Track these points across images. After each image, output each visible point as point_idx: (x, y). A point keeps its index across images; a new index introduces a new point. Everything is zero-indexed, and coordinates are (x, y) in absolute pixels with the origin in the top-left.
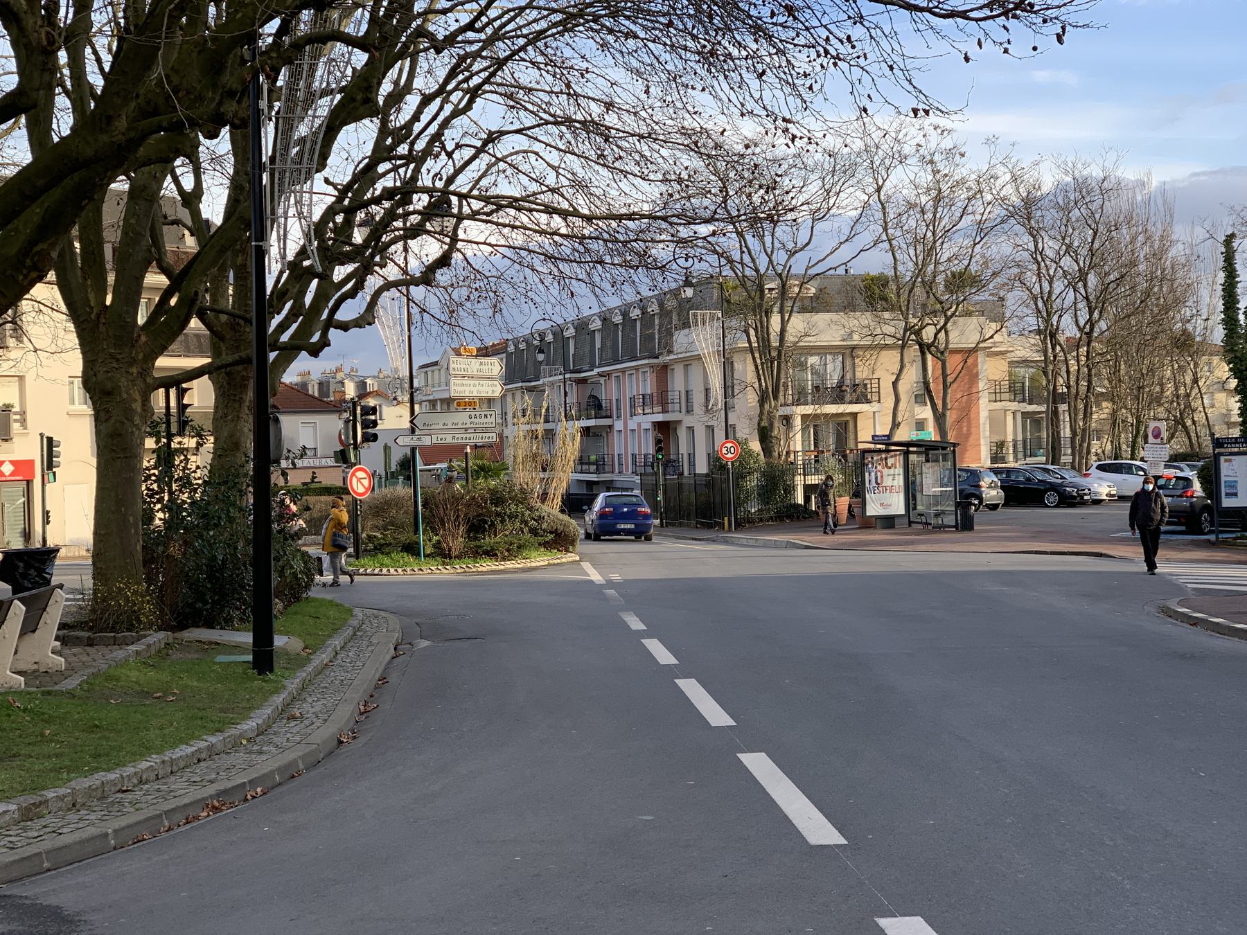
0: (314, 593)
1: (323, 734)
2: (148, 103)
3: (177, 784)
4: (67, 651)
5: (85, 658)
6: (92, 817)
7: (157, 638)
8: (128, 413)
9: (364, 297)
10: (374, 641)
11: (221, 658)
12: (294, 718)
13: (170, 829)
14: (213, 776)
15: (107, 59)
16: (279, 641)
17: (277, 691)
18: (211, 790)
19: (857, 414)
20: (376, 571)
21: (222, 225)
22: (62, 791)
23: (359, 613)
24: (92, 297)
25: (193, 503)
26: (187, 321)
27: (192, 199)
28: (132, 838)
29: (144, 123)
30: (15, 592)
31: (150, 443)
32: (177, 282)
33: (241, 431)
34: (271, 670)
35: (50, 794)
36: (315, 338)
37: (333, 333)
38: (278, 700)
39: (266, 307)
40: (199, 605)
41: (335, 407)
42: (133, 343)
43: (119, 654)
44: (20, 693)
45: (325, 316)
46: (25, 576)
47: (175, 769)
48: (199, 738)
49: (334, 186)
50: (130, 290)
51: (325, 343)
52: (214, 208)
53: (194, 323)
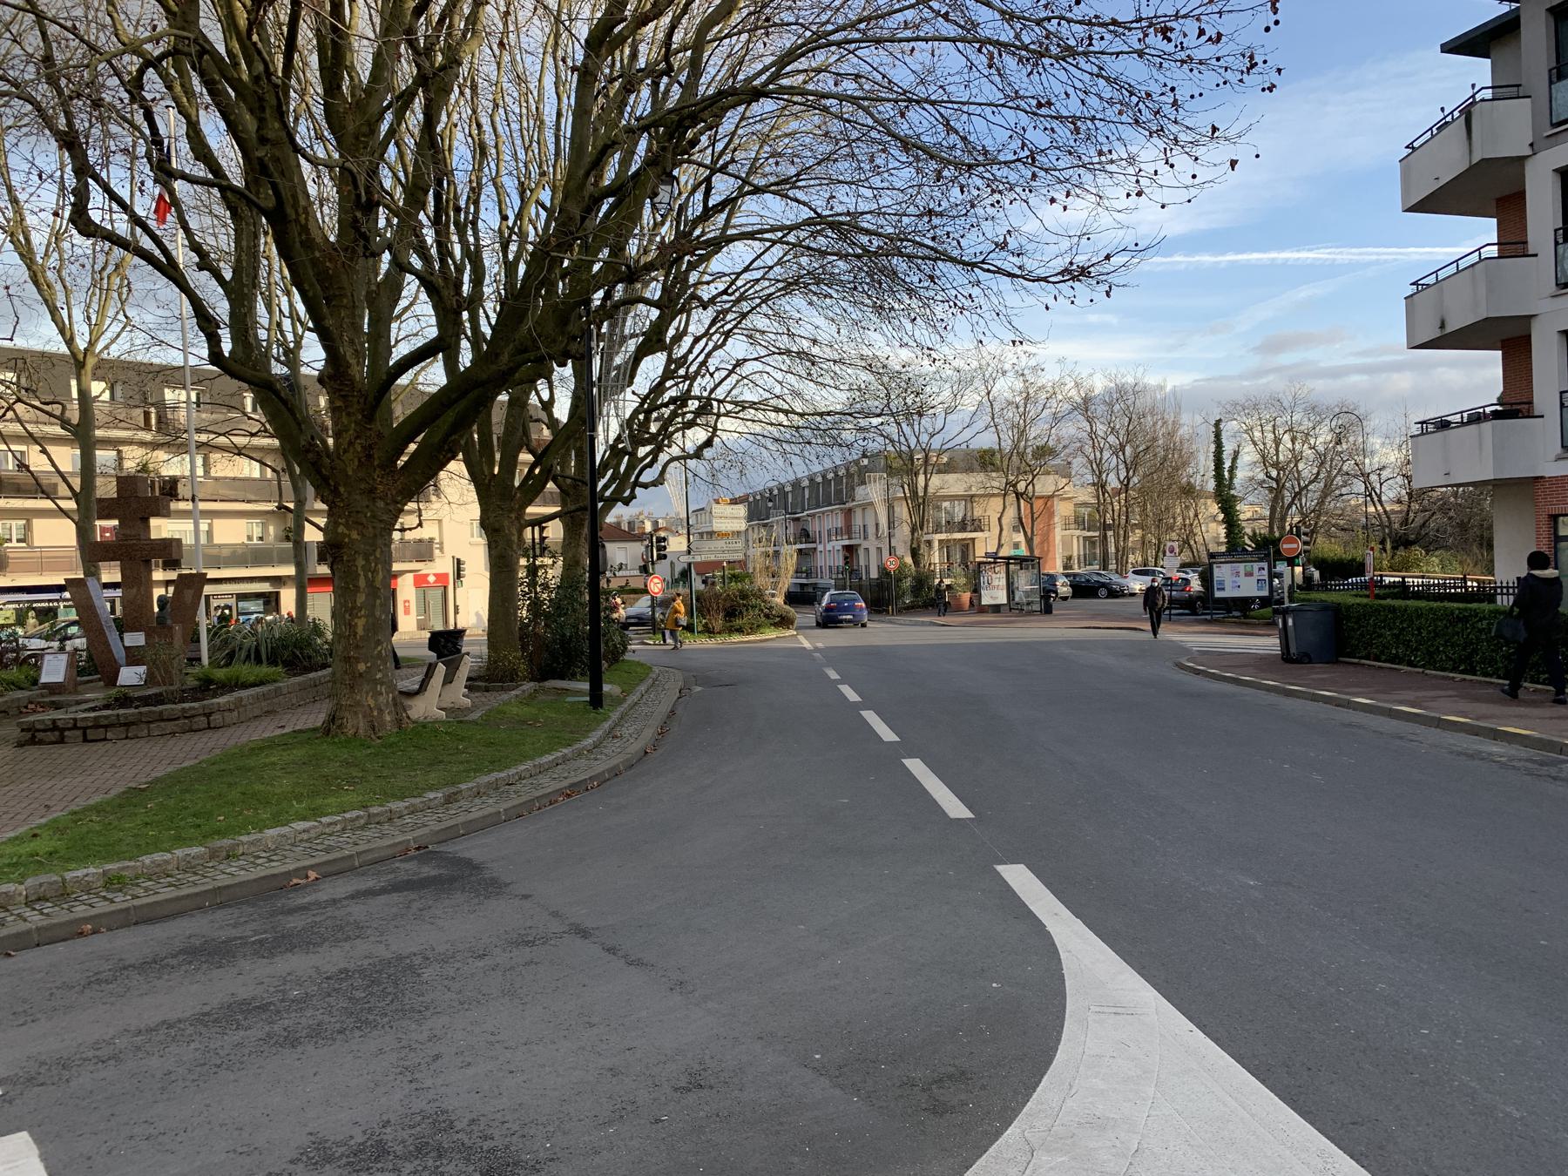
0: (628, 656)
1: (635, 747)
3: (544, 780)
6: (491, 801)
7: (529, 686)
8: (509, 543)
9: (658, 467)
11: (569, 699)
16: (606, 688)
18: (566, 783)
22: (470, 785)
23: (657, 670)
27: (548, 406)
28: (516, 814)
29: (519, 358)
31: (523, 562)
35: (463, 787)
36: (627, 493)
37: (638, 490)
38: (606, 725)
39: (596, 474)
41: (639, 538)
42: (512, 498)
43: (505, 696)
45: (633, 479)
47: (542, 770)
49: (638, 396)
50: (510, 464)
51: (633, 496)
52: (562, 411)
53: (550, 485)
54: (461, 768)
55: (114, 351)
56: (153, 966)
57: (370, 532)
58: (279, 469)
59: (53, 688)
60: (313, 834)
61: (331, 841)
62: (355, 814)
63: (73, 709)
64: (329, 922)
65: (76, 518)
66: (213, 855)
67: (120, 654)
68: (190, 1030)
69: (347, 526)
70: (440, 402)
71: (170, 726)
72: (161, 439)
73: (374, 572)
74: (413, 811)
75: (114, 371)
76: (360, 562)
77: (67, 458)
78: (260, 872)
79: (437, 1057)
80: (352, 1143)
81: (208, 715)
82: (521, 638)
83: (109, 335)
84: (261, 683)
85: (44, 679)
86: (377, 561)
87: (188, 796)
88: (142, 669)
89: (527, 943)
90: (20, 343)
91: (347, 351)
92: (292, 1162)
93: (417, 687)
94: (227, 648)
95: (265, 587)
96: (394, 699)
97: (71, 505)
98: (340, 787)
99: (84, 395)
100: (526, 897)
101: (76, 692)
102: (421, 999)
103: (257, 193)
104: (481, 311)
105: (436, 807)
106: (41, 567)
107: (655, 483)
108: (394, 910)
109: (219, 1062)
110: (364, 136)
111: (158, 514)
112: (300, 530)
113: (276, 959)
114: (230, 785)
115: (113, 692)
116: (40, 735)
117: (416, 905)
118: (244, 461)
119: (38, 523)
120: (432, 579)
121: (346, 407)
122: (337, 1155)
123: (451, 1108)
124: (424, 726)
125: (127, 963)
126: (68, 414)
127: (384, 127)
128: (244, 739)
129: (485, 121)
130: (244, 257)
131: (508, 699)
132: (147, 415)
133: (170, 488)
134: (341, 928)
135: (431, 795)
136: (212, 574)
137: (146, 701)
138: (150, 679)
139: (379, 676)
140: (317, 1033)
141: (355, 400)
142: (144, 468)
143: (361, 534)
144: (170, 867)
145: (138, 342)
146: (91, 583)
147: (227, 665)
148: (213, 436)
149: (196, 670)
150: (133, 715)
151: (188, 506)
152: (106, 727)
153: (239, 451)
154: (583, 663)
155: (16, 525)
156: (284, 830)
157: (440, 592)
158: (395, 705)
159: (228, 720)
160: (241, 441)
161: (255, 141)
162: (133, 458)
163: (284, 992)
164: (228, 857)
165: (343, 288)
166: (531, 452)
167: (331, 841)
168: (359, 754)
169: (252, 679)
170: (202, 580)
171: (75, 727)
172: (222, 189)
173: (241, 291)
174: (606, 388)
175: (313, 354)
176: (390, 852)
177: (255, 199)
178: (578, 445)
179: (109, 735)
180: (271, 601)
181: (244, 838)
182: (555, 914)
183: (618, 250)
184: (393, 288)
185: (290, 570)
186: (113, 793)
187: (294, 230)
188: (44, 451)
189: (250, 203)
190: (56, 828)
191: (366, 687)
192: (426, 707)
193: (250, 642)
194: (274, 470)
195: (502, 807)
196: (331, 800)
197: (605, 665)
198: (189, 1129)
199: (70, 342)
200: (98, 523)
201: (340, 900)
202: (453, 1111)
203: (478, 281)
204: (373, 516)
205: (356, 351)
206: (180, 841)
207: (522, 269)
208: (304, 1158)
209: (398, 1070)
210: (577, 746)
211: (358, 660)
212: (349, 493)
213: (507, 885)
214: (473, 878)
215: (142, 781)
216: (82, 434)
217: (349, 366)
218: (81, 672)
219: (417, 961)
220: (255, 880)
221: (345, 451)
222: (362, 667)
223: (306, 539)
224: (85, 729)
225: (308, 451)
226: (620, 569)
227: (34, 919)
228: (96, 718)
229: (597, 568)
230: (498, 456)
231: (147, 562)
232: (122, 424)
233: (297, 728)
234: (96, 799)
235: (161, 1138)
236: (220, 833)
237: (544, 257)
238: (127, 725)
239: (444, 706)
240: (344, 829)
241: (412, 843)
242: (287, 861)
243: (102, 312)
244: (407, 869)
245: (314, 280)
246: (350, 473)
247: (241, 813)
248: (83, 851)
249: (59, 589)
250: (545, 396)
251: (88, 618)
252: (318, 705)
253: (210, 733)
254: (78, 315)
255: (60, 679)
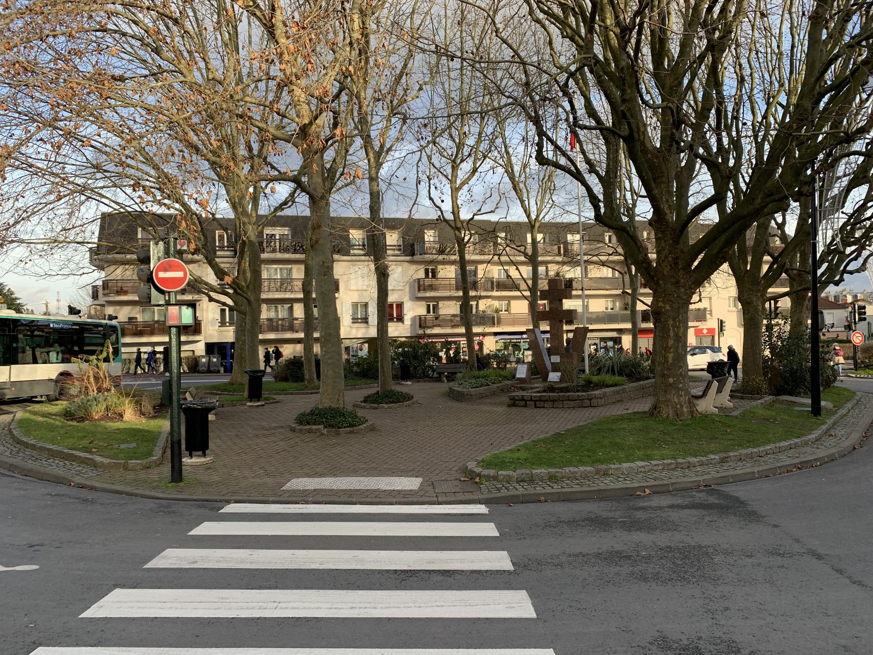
0: (836, 384)
1: (847, 444)
2: (769, 191)
3: (783, 457)
4: (732, 401)
5: (740, 404)
6: (748, 465)
7: (769, 398)
8: (756, 310)
9: (861, 260)
10: (867, 406)
11: (796, 408)
12: (831, 435)
13: (780, 474)
14: (797, 455)
15: (747, 179)
16: (823, 403)
17: (824, 423)
18: (797, 461)
19: (367, 323)
20: (866, 376)
21: (795, 236)
22: (736, 454)
23: (859, 394)
24: (742, 267)
25: (783, 346)
26: (781, 274)
27: (781, 226)
28: (765, 475)
29: (768, 199)
30: (713, 377)
31: (765, 322)
32: (775, 260)
33: (803, 317)
34: (820, 415)
35: (731, 454)
36: (837, 278)
37: (846, 276)
38: (824, 427)
39: (816, 265)
40: (786, 386)
41: (844, 306)
42: (759, 283)
43: (754, 403)
44: (715, 415)
45: (842, 268)
46: (717, 371)
47: (781, 450)
48: (790, 439)
49: (846, 214)
50: (758, 263)
51: (842, 280)
52: (791, 229)
53: (784, 275)
54: (729, 443)
55: (547, 219)
56: (572, 523)
57: (676, 305)
58: (623, 272)
59: (521, 380)
60: (647, 469)
61: (657, 474)
62: (669, 461)
63: (530, 391)
64: (658, 519)
65: (530, 299)
66: (597, 472)
67: (549, 366)
68: (593, 560)
69: (663, 302)
70: (715, 232)
71: (572, 404)
72: (566, 259)
73: (678, 328)
74: (702, 464)
75: (547, 228)
76: (671, 322)
77: (526, 271)
78: (620, 485)
79: (727, 609)
80: (681, 643)
81: (590, 400)
82: (763, 368)
83: (545, 210)
84: (615, 385)
85: (518, 376)
86: (680, 321)
87: (584, 440)
88: (559, 374)
89: (779, 554)
90: (509, 219)
91: (665, 207)
92: (650, 643)
93: (701, 393)
94: (598, 365)
95: (614, 334)
96: (689, 399)
97: (527, 294)
98: (660, 446)
99: (534, 240)
100: (776, 526)
101: (531, 383)
102: (714, 572)
103: (620, 129)
104: (740, 176)
105: (715, 464)
106: (514, 323)
107: (858, 271)
108: (694, 519)
109: (608, 580)
110: (675, 86)
111: (566, 298)
112: (634, 305)
113: (632, 533)
114: (603, 437)
115: (547, 384)
116: (517, 402)
117: (707, 519)
118: (605, 269)
119: (514, 303)
120: (705, 331)
121: (664, 237)
122: (674, 647)
123: (738, 641)
124: (706, 417)
125: (562, 520)
126: (527, 251)
127: (686, 82)
128: (608, 414)
129: (744, 61)
130: (611, 163)
131: (756, 405)
132: (559, 248)
133: (569, 283)
134: (665, 523)
135: (713, 457)
136: (591, 327)
137: (562, 390)
138: (562, 379)
139: (681, 386)
140: (656, 577)
141: (669, 233)
142: (558, 274)
143: (671, 307)
144: (577, 475)
145: (557, 213)
146: (536, 330)
147: (598, 374)
148: (590, 257)
149: (583, 376)
150: (555, 396)
151: (580, 293)
152: (544, 401)
153: (603, 264)
154: (806, 386)
155: (505, 303)
156: (632, 465)
157: (710, 339)
158: (690, 403)
159: (599, 404)
160: (604, 258)
161: (619, 100)
162: (553, 269)
163: (638, 551)
164: (604, 474)
165: (663, 172)
166: (769, 255)
167: (657, 474)
168: (670, 429)
169: (611, 383)
170: (587, 330)
171: (531, 400)
172: (601, 130)
173: (610, 181)
174: (825, 212)
175: (644, 210)
176: (689, 485)
177: (618, 132)
178: (802, 249)
179: (546, 406)
180: (617, 341)
181: (613, 466)
182: (797, 541)
183: (836, 125)
184: (690, 166)
185: (629, 326)
186: (549, 434)
187: (638, 145)
188: (517, 269)
189: (614, 133)
190: (527, 448)
191: (673, 392)
192: (706, 405)
193: (609, 363)
194: (620, 273)
195: (756, 469)
196: (656, 452)
197: (821, 389)
198: (597, 610)
199: (528, 216)
200: (539, 302)
201: (664, 508)
202: (739, 643)
203: (738, 159)
204: (678, 297)
205: (670, 206)
206: (582, 462)
207: (767, 147)
208: (656, 643)
209: (705, 610)
210: (804, 438)
211: (669, 377)
212: (665, 284)
213: (763, 517)
214: (740, 509)
215: (561, 430)
216: (533, 261)
217: (666, 214)
218: (532, 374)
219: (710, 550)
220: (619, 489)
221: (663, 261)
222: (671, 380)
223: (638, 309)
224: (535, 401)
225: (643, 262)
226: (832, 327)
227: (520, 490)
228: (540, 396)
229: (817, 326)
230: (750, 259)
231: (561, 321)
232: (549, 254)
233: (635, 411)
234: (542, 436)
235: (584, 611)
236: (601, 462)
237: (786, 135)
238: (554, 401)
239: (717, 405)
240: (663, 469)
241: (702, 483)
242: (634, 481)
243: (542, 201)
244: (700, 497)
245: (647, 170)
246: (666, 273)
247: (610, 453)
248: (539, 461)
249: (522, 333)
250: (780, 220)
251: (534, 346)
252: (645, 399)
253: (591, 409)
254: (533, 202)
255: (524, 376)
